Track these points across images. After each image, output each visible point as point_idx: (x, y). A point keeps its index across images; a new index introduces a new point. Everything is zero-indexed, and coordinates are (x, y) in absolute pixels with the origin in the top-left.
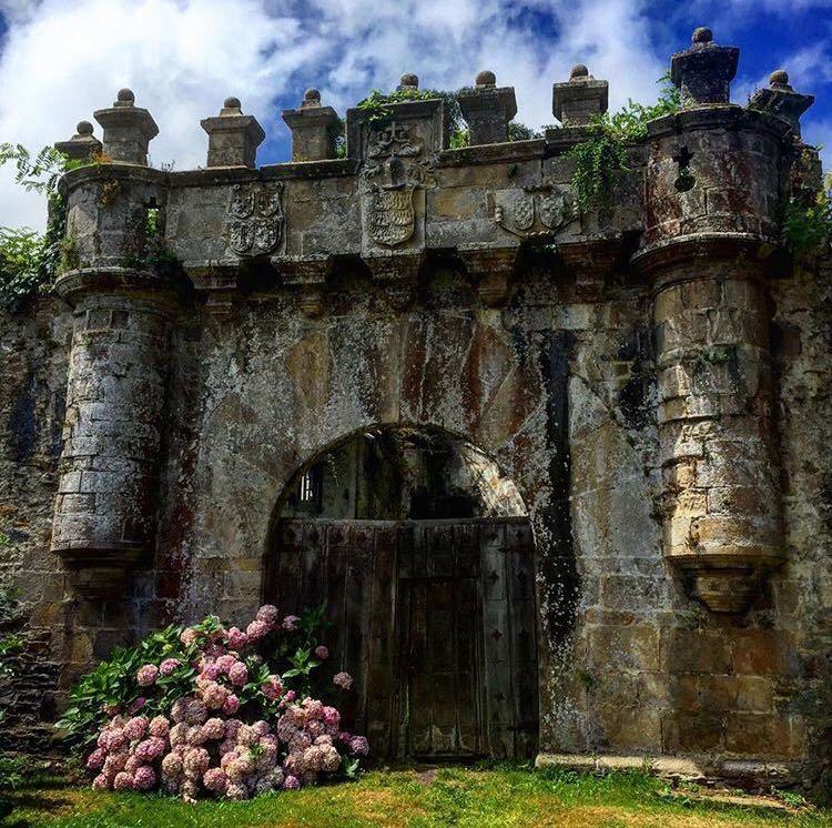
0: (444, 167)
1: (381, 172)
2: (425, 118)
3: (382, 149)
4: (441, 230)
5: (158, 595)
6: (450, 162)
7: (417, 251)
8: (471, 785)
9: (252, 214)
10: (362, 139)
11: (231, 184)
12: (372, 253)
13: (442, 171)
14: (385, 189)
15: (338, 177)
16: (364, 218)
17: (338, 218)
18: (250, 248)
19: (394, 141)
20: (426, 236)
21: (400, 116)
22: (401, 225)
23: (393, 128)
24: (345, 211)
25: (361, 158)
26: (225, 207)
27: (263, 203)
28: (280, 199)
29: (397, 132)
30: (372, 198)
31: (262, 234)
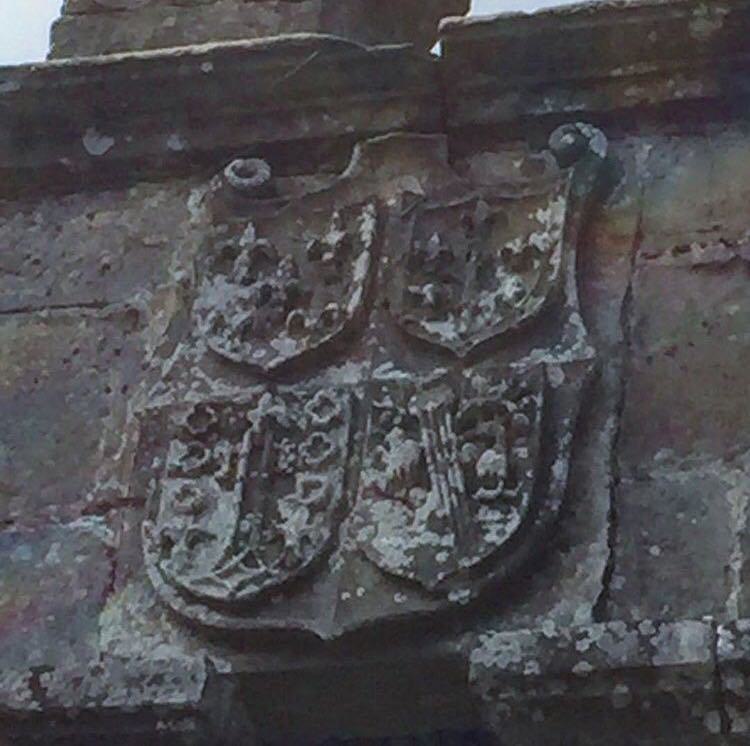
5: (294, 491)
9: (343, 344)
11: (200, 164)
18: (301, 581)
26: (134, 317)
27: (443, 269)
28: (583, 235)
31: (418, 475)
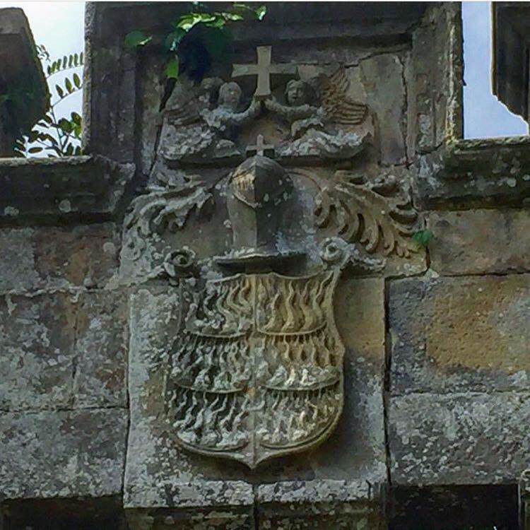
0: (460, 203)
1: (210, 212)
2: (381, 44)
3: (219, 135)
4: (446, 418)
6: (482, 186)
7: (357, 488)
8: (223, 89)
10: (140, 106)
12: (170, 492)
13: (451, 216)
14: (229, 268)
15: (41, 222)
16: (138, 369)
17: (34, 367)
19: (264, 112)
20: (390, 440)
21: (286, 34)
22: (295, 393)
23: (263, 66)
24: (62, 342)
25: (137, 158)
29: (279, 83)
30: (172, 299)
